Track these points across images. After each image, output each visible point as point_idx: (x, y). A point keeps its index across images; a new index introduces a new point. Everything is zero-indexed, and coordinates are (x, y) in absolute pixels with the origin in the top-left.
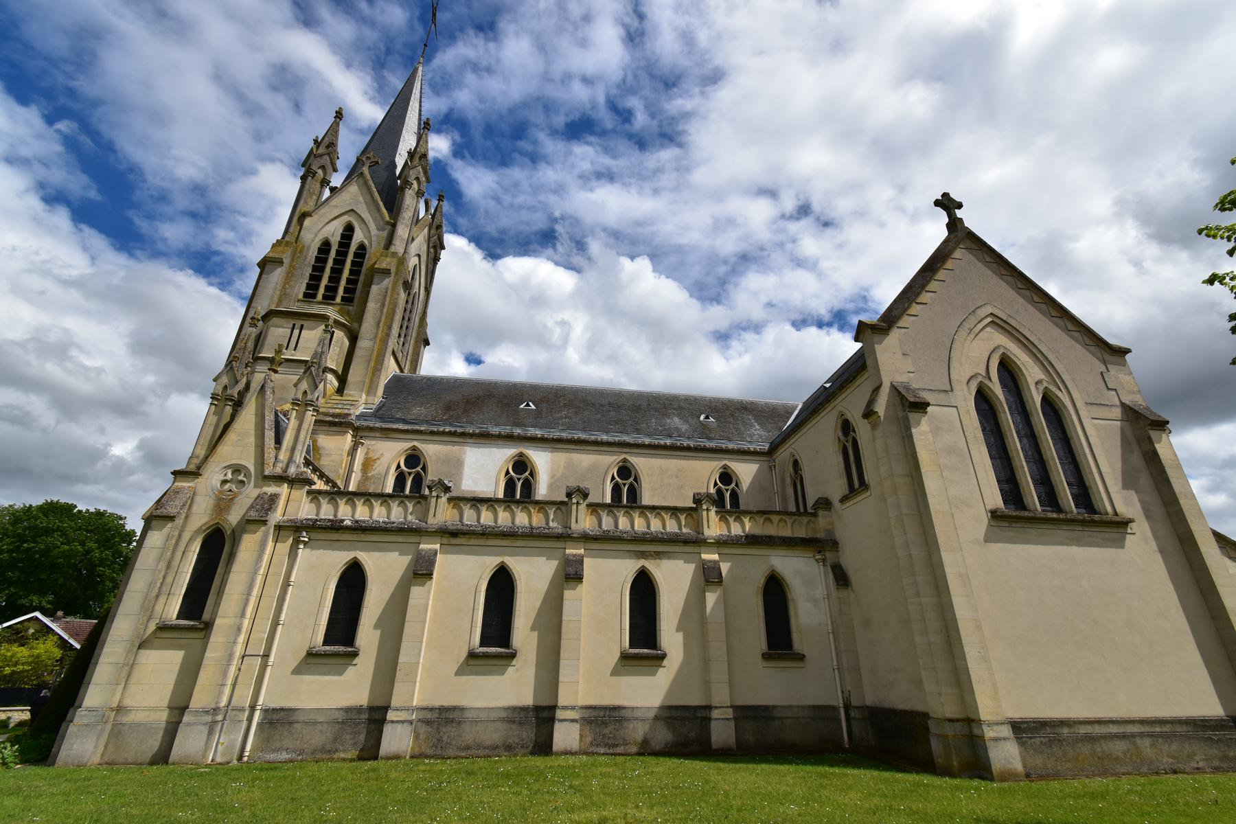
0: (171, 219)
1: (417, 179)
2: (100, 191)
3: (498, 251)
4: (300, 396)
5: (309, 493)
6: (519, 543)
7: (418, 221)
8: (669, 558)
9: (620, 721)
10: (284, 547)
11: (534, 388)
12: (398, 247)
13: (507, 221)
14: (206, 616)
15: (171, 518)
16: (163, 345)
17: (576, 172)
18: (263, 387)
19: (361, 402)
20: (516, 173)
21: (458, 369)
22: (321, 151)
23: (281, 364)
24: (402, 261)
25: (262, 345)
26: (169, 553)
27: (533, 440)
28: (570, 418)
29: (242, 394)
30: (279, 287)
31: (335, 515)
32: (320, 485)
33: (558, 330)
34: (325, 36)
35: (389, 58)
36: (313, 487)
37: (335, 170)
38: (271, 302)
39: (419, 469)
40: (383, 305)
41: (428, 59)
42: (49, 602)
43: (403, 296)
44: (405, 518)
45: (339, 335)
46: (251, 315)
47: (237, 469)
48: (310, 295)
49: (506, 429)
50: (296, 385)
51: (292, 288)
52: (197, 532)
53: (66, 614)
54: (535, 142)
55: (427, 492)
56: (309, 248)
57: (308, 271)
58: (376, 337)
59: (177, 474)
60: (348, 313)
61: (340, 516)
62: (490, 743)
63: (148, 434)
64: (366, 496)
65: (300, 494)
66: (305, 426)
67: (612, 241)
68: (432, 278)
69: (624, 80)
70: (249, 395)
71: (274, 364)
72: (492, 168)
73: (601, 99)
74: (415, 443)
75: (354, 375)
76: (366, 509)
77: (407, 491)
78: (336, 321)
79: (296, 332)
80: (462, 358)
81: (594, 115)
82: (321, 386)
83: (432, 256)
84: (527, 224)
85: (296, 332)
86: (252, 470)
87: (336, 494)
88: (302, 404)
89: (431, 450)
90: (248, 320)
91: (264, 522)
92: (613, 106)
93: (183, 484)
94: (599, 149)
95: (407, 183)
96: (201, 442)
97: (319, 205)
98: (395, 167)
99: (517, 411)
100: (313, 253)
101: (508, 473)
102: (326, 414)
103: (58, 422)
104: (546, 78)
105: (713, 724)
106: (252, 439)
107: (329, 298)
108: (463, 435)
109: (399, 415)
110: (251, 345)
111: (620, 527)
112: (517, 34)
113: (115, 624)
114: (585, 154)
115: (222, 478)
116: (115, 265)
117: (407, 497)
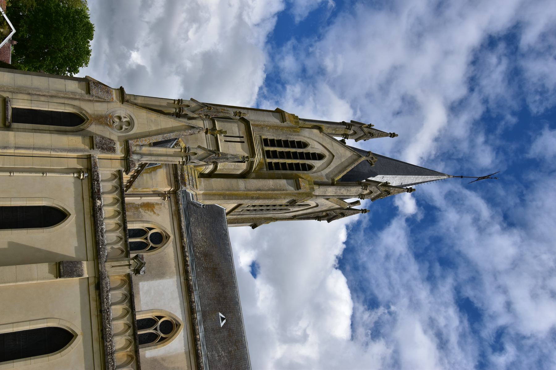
0: (297, 60)
1: (371, 192)
2: (301, 22)
3: (348, 268)
4: (192, 151)
5: (120, 172)
6: (96, 346)
7: (342, 199)
10: (74, 164)
11: (239, 321)
12: (318, 191)
13: (374, 269)
14: (15, 125)
15: (88, 92)
16: (211, 67)
17: (434, 315)
18: (193, 127)
19: (197, 192)
20: (413, 268)
21: (242, 259)
22: (365, 129)
23: (213, 135)
24: (309, 195)
25: (223, 121)
26: (62, 95)
27: (193, 332)
28: (220, 360)
29: (185, 116)
30: (266, 123)
31: (103, 193)
32: (126, 178)
33: (299, 333)
34: (449, 122)
35: (455, 161)
36: (124, 174)
37: (356, 140)
38: (255, 121)
39: (151, 244)
40: (274, 190)
41: (468, 187)
42: (23, 36)
43: (284, 202)
44: (108, 244)
45: (243, 167)
46: (242, 111)
47: (130, 124)
48: (266, 142)
49: (198, 307)
50: (199, 147)
51: (268, 131)
52: (80, 109)
53: (15, 46)
54: (443, 277)
55: (132, 255)
56: (298, 135)
57: (283, 138)
58: (249, 190)
59: (121, 90)
60: (261, 169)
61: (103, 197)
63: (149, 69)
64: (123, 210)
65: (118, 166)
66: (170, 159)
67: (389, 361)
68: (301, 219)
69: (524, 337)
70: (186, 120)
71: (213, 131)
72: (410, 248)
73: (502, 321)
74: (172, 237)
75: (216, 183)
76: (112, 214)
77: (131, 240)
78: (252, 163)
79: (238, 139)
80: (254, 259)
81: (486, 319)
82: (202, 163)
83: (320, 215)
84: (378, 285)
85: (238, 139)
86: (132, 132)
87: (121, 190)
88: (187, 154)
89: (169, 251)
90: (238, 110)
91: (92, 147)
92: (500, 333)
93: (115, 95)
94: (460, 330)
95: (365, 186)
96: (146, 99)
97: (330, 136)
98: (374, 176)
99: (216, 311)
100: (296, 138)
101: (160, 317)
102: (182, 170)
103: (147, 23)
104: (496, 274)
106: (154, 128)
107: (268, 154)
108: (186, 272)
109: (192, 220)
110: (221, 115)
111: (113, 307)
112: (514, 244)
113: (7, 73)
114: (451, 319)
115: (122, 116)
116: (259, 36)
117: (126, 241)
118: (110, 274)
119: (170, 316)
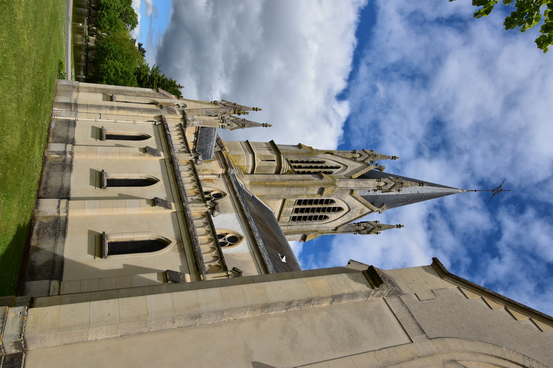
6: (173, 186)
8: (181, 256)
9: (55, 235)
62: (49, 181)
105: (46, 282)
118: (191, 209)
119: (234, 233)
